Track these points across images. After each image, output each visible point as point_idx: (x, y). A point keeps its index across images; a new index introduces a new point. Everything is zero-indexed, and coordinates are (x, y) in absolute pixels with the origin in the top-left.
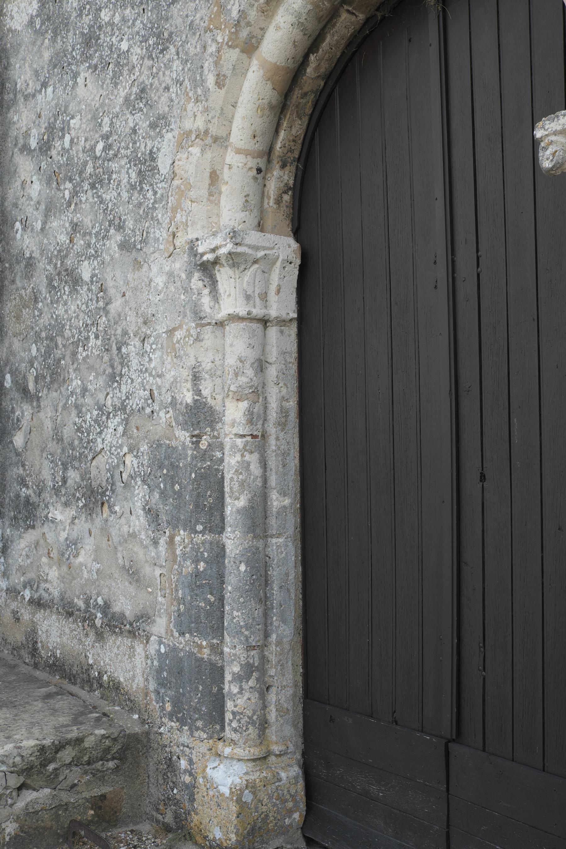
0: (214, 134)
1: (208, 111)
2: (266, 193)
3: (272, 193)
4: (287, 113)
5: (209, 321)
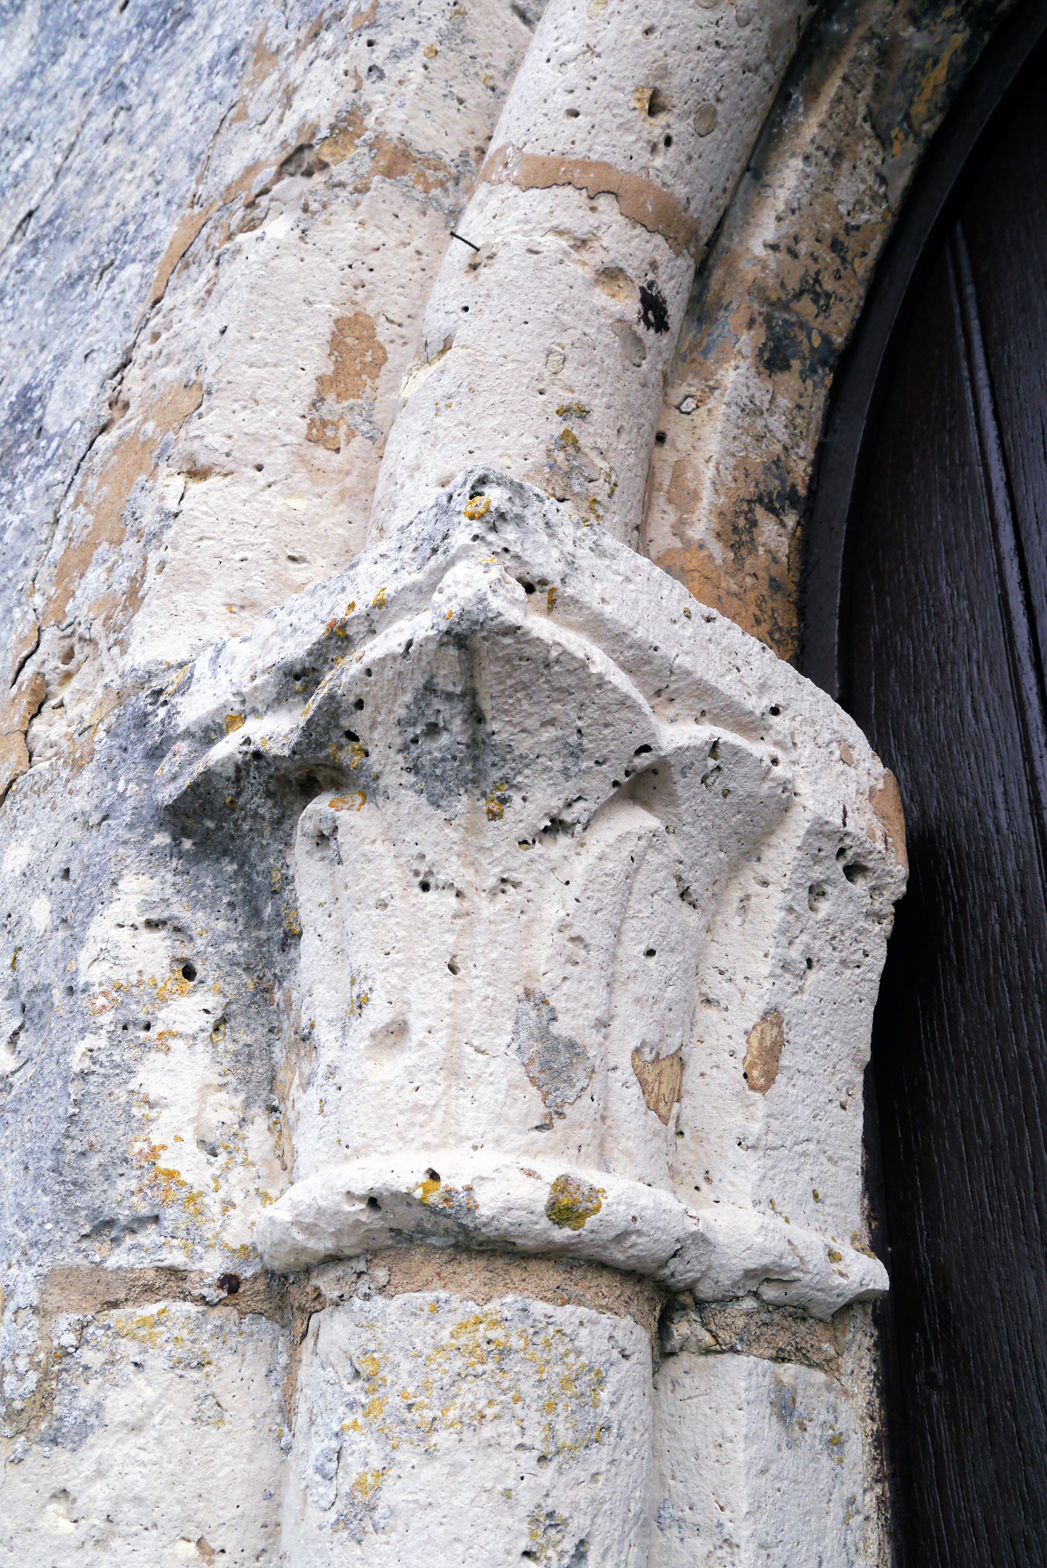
0: (393, 130)
1: (373, 24)
2: (665, 477)
3: (709, 472)
4: (826, 74)
5: (175, 1258)
